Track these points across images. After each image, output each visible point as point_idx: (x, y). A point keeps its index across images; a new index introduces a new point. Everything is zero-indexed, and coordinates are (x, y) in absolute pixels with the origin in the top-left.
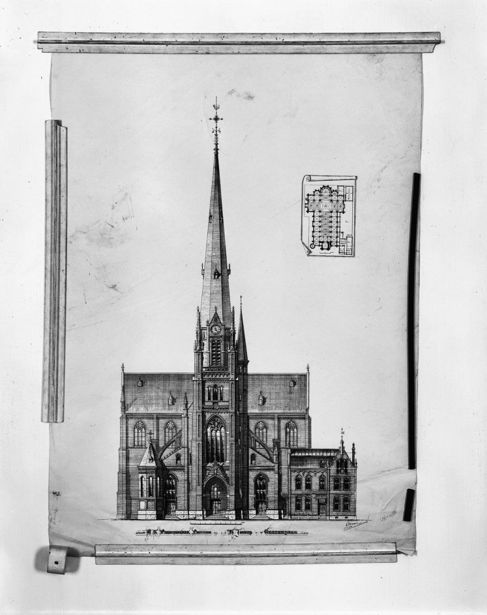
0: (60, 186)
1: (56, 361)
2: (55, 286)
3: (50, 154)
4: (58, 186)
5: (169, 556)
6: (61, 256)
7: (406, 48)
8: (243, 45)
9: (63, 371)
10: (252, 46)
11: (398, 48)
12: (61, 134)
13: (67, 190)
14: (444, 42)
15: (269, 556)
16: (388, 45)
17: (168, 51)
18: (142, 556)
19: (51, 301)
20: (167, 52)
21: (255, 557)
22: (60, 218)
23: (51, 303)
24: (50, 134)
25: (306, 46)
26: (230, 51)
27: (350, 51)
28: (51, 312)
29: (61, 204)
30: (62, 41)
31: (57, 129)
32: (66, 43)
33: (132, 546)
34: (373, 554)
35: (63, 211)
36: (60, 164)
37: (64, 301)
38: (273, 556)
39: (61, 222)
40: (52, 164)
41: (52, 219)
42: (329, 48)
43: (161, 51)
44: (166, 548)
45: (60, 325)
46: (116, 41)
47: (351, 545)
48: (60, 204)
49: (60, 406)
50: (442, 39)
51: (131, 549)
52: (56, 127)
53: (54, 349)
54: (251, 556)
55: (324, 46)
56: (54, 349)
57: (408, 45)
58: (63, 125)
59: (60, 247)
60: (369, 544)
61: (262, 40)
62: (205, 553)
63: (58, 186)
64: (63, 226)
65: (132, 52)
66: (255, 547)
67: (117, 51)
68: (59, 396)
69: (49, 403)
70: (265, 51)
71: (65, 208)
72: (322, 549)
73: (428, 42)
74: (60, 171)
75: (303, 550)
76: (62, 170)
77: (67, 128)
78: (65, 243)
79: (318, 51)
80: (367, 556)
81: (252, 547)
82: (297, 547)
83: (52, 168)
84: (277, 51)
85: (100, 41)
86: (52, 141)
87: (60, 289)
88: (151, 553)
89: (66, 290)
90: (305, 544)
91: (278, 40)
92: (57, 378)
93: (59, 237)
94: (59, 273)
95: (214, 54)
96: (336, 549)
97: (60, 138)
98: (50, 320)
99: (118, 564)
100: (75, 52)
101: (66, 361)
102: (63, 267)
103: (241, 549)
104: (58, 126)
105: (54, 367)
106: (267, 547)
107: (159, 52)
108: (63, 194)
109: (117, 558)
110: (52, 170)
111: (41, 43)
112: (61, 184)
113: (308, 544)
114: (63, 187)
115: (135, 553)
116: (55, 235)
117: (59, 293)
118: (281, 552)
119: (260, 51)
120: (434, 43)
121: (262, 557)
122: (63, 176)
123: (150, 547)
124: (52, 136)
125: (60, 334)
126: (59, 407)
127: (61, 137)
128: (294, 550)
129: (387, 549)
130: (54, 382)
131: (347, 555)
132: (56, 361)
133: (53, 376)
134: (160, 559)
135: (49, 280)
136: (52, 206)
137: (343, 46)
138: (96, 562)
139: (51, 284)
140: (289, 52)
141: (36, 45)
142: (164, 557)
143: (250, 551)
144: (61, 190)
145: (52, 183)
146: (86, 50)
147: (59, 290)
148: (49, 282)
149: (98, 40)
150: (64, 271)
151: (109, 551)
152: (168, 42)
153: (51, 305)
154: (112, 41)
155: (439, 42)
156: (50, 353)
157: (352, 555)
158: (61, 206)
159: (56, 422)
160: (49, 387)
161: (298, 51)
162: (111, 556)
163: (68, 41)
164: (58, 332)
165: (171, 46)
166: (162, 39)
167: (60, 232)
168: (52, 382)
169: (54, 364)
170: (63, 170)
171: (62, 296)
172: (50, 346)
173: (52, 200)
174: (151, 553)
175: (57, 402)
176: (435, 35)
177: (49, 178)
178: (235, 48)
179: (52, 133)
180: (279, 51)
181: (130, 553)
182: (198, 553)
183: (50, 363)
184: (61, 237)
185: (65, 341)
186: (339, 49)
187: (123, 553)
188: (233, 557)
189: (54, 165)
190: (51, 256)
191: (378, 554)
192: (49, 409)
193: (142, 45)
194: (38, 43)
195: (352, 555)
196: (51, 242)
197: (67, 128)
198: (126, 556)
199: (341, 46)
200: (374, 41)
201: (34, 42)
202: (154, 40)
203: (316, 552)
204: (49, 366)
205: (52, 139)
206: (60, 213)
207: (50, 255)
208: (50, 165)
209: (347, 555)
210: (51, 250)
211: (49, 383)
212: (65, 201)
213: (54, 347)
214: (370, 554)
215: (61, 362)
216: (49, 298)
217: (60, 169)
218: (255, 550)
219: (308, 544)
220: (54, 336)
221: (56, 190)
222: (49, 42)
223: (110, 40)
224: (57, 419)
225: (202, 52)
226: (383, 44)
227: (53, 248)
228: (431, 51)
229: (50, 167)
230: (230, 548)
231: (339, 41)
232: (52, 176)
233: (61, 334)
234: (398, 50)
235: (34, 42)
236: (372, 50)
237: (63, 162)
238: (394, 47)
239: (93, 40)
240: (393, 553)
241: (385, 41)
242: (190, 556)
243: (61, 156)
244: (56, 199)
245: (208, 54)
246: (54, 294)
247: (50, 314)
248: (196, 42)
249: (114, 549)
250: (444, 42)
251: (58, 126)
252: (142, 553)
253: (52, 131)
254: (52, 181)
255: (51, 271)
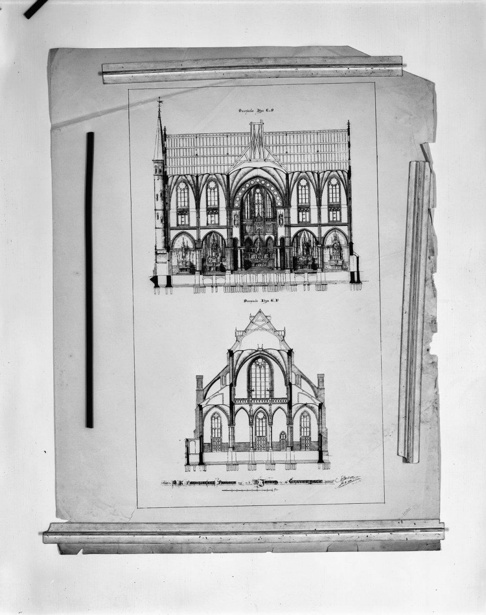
0: (406, 398)
1: (415, 223)
2: (413, 297)
3: (415, 430)
4: (408, 396)
5: (329, 66)
6: (407, 328)
7: (77, 528)
8: (240, 532)
9: (409, 212)
10: (230, 531)
11: (85, 528)
12: (403, 449)
13: (400, 393)
14: (40, 533)
15: (230, 67)
16: (95, 531)
17: (314, 524)
18: (355, 65)
19: (419, 282)
20: (315, 524)
21: (244, 66)
22: (407, 366)
23: (419, 280)
24: (414, 450)
25: (177, 530)
26: (253, 525)
27: (134, 526)
28: (419, 272)
29: (405, 379)
30: (420, 530)
31: (408, 453)
32: (416, 529)
33: (366, 75)
34: (126, 71)
35: (404, 372)
36: (405, 419)
37: (406, 282)
38: (225, 67)
39: (406, 361)
40: (414, 419)
41: (415, 365)
42: (154, 528)
43: (321, 524)
44: (332, 74)
45: (410, 258)
46: (366, 532)
47: (147, 80)
48: (407, 379)
49: (413, 177)
50: (41, 537)
51: (367, 72)
52: (408, 456)
53: (417, 234)
54: (248, 67)
55: (160, 531)
56: (417, 234)
57: (75, 531)
58: (402, 458)
59: (408, 337)
60: (130, 81)
61: (221, 536)
62: (293, 69)
63: (408, 396)
64: (404, 357)
65: (351, 522)
66: (243, 75)
67: (365, 522)
68: (414, 187)
69: (424, 181)
70: (218, 525)
71: (401, 375)
72: (176, 76)
73: (56, 533)
74: (406, 412)
75: (196, 75)
76: (404, 413)
77: (398, 455)
78: (403, 340)
79: (165, 525)
80: (132, 69)
81: (246, 75)
82: (201, 77)
83: (414, 416)
84: (206, 525)
85: (382, 532)
86: (413, 442)
87: (409, 294)
88: (347, 69)
89: (403, 293)
90: (194, 80)
91: (204, 537)
92: (415, 205)
93: (408, 346)
94: (410, 310)
95: (268, 522)
96: (163, 76)
97: (405, 444)
98: (420, 264)
99: (379, 57)
100: (407, 521)
101: (405, 223)
102: (406, 316)
103: (258, 74)
104: (406, 457)
105: (417, 217)
106: (231, 76)
107: (324, 524)
108: (403, 389)
109: (381, 63)
110: (414, 413)
111: (441, 528)
112: (405, 399)
113: (191, 80)
114: (403, 396)
115: (363, 69)
116: (412, 347)
117: (410, 290)
118: (217, 71)
119: (222, 525)
120: (50, 532)
121: (237, 66)
122: (403, 407)
123: (349, 74)
124: (413, 446)
125: (411, 250)
126: (414, 177)
127: (403, 447)
128: (205, 74)
129: (111, 77)
130: (418, 202)
131: (152, 70)
132: (415, 223)
133: (419, 208)
134: (338, 62)
135: (419, 304)
136: (415, 378)
137: (140, 531)
138: (402, 59)
139: (418, 300)
140: (194, 525)
141: (446, 527)
142: (334, 65)
143: (248, 72)
144: (405, 393)
145: (414, 400)
146: (396, 523)
147: (410, 293)
148: (420, 302)
149: (385, 533)
150: (404, 312)
151: (389, 70)
152: (315, 533)
153: (419, 278)
154: (370, 532)
155: (45, 533)
156: (421, 230)
157: (147, 70)
158: (405, 377)
159: (417, 162)
160: (423, 196)
161: (185, 526)
162: (387, 65)
163: (415, 530)
164: (412, 251)
165: (311, 529)
166: (321, 536)
167: (408, 351)
168: (420, 201)
169: (417, 219)
170: (402, 414)
171: (407, 288)
172: (421, 238)
173: (415, 384)
174: (347, 69)
175: (416, 182)
176: (48, 541)
177: (417, 405)
178: (247, 528)
179: (413, 450)
180: (204, 525)
181: (368, 68)
182: (300, 69)
183: (422, 221)
184: (406, 346)
185: (406, 242)
186: (144, 528)
187: (375, 68)
188: (265, 66)
189: (411, 418)
190: (417, 327)
191: (121, 71)
192: (424, 174)
193: (345, 529)
194: (444, 529)
195: (147, 70)
196: (416, 342)
197: (398, 455)
198: (372, 65)
199: (143, 531)
200: (109, 535)
201: (448, 529)
202: (329, 534)
203: (183, 73)
204: (422, 218)
205: (413, 444)
206: (407, 370)
207: (418, 328)
208: (415, 418)
209: (152, 70)
210: (417, 334)
211: (423, 201)
212: (402, 382)
213: (416, 237)
214: (129, 71)
215: (411, 222)
216: (420, 285)
217: (406, 414)
218: (244, 73)
219: (191, 80)
220: (417, 248)
221: (410, 393)
222: (433, 530)
223: (372, 534)
224: (416, 164)
225: (281, 524)
226: (100, 532)
227: (415, 336)
228: (52, 525)
229: (415, 416)
230: (269, 75)
231: (144, 535)
232: (414, 407)
233: (409, 250)
234: (86, 525)
235: (448, 529)
236: (111, 526)
237: (402, 421)
238: (89, 529)
239: (389, 533)
240: (106, 73)
241: (99, 535)
242: (308, 66)
243: (404, 427)
244: (411, 384)
245: (274, 523)
246: (415, 289)
247: (419, 269)
248: (286, 534)
249: (384, 72)
250: (40, 533)
251: (406, 457)
252: (356, 69)
253: (413, 452)
254: (414, 402)
255: (417, 313)
